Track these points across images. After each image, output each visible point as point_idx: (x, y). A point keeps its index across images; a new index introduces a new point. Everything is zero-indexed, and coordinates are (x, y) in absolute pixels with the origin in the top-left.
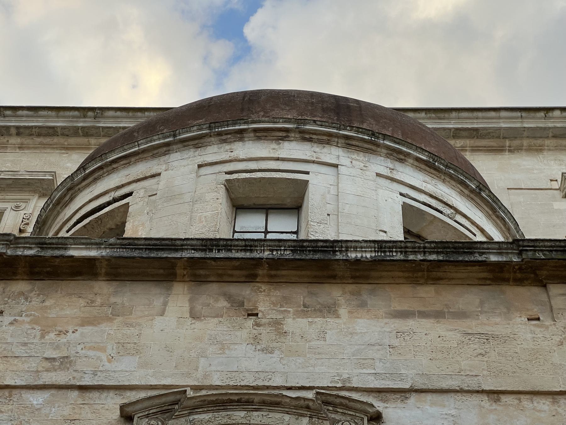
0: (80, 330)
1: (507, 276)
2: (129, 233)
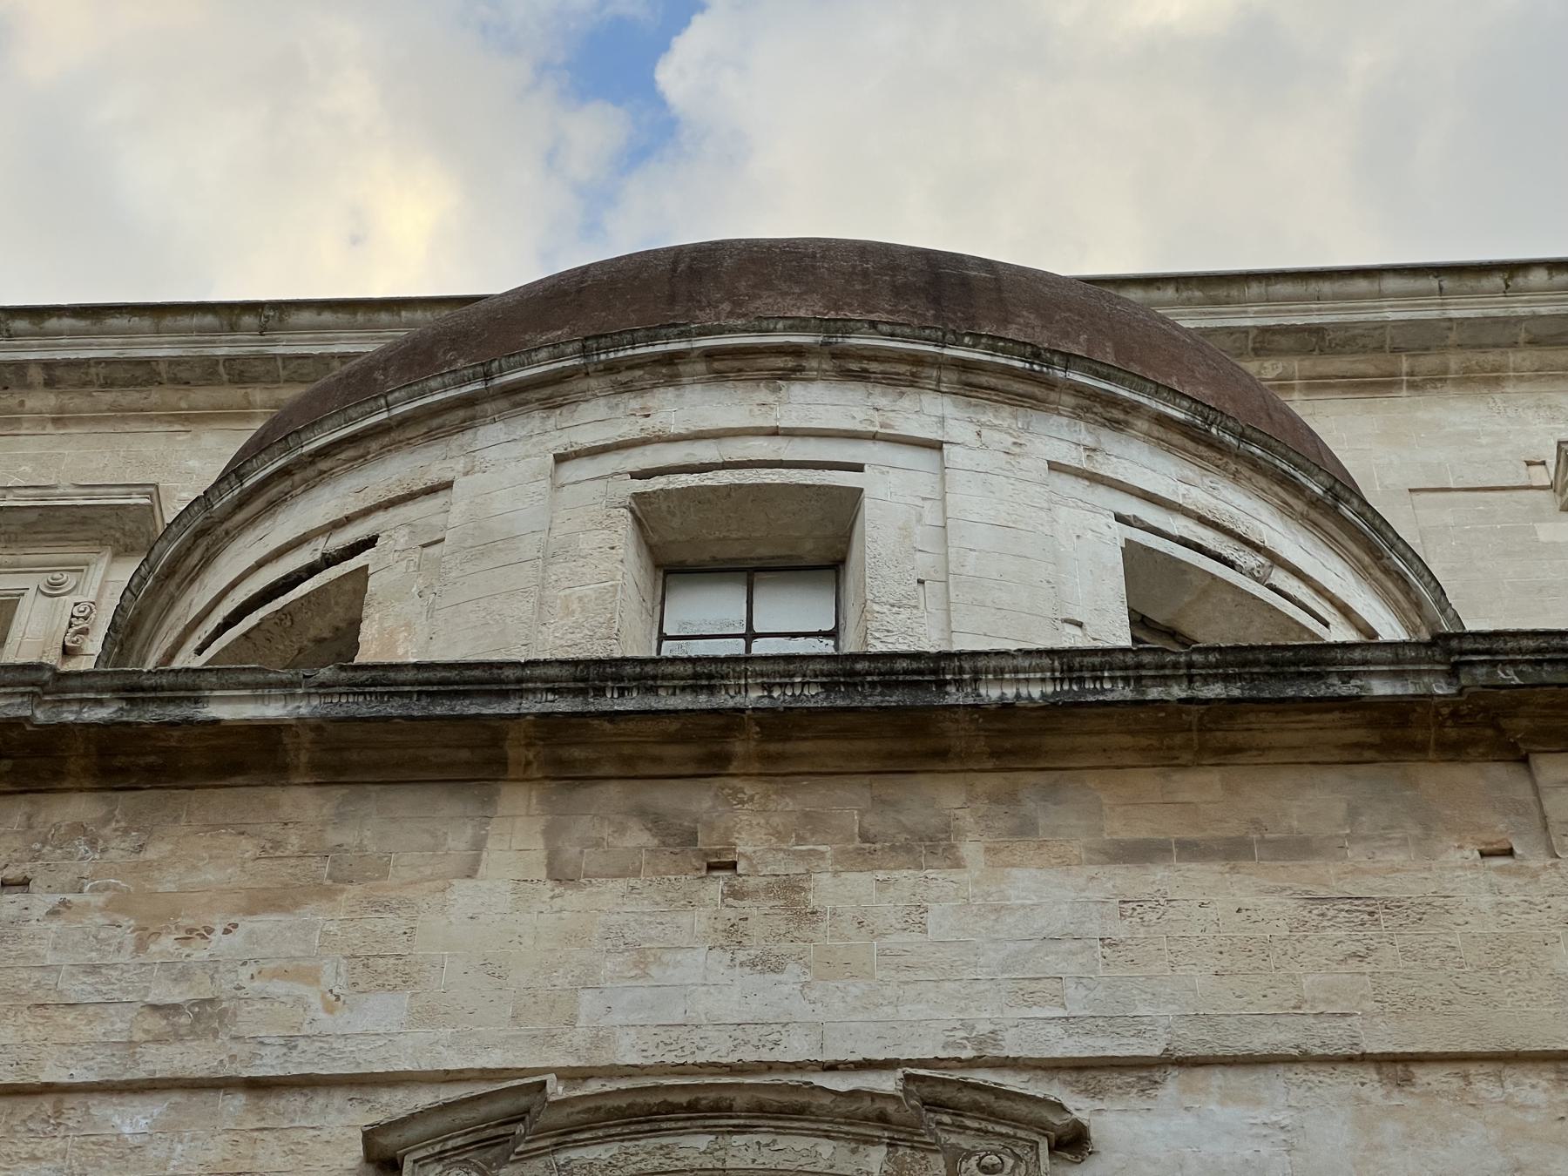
0: (247, 924)
1: (1419, 735)
2: (370, 651)
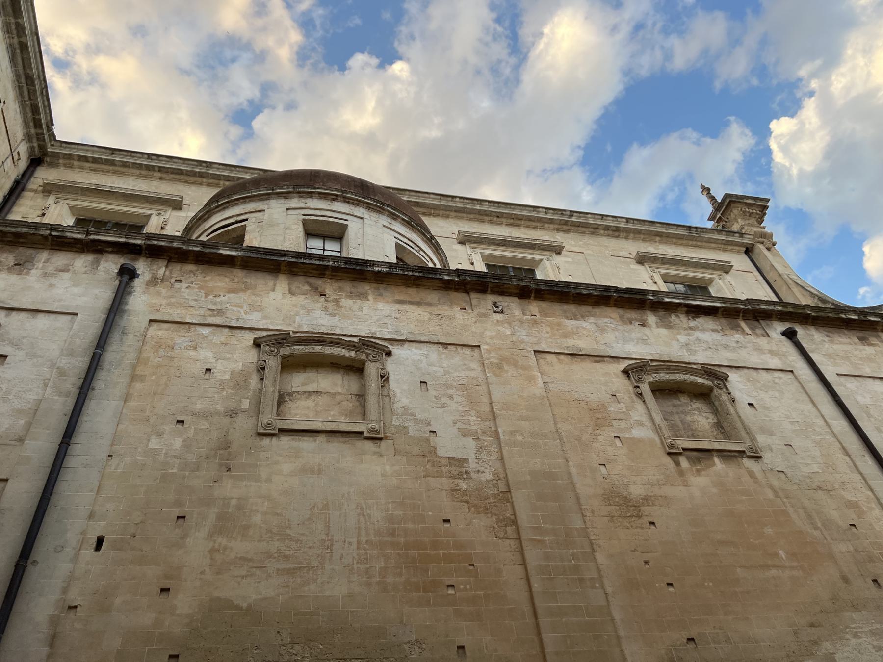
0: (228, 295)
1: (451, 286)
2: (247, 243)
